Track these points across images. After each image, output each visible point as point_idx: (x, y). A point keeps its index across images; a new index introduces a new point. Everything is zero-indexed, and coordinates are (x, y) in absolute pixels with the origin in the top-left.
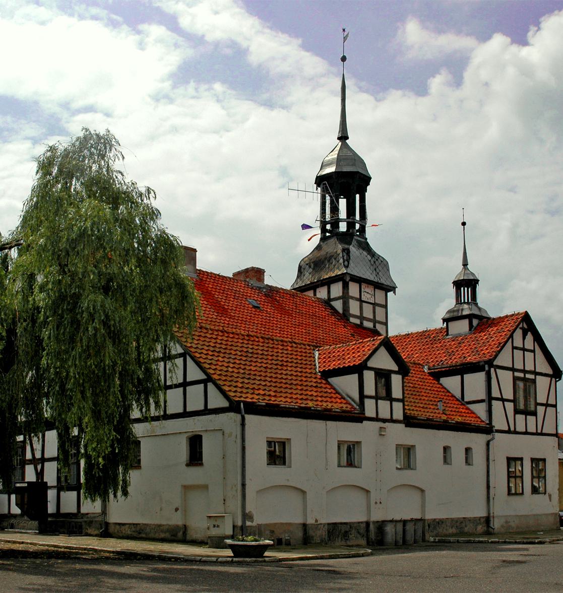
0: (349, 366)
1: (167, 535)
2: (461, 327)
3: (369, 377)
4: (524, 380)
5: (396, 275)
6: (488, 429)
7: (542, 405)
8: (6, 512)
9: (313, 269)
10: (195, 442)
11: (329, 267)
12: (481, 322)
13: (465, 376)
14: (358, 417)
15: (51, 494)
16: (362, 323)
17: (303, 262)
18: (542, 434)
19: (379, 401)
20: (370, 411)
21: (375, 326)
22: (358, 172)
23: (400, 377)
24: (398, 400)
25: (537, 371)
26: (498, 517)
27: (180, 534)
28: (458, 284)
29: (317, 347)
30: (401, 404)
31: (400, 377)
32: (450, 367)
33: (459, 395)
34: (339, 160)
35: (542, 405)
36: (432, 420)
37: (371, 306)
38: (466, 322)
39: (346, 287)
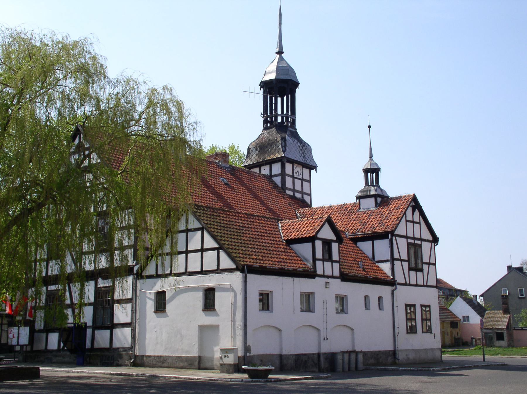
0: (306, 237)
1: (186, 364)
2: (369, 204)
3: (319, 244)
4: (414, 245)
5: (317, 157)
6: (392, 283)
7: (426, 263)
8: (43, 348)
9: (259, 151)
10: (209, 294)
11: (271, 151)
12: (383, 200)
13: (375, 242)
14: (311, 274)
15: (89, 332)
16: (294, 194)
17: (251, 146)
18: (427, 286)
19: (325, 263)
20: (319, 271)
21: (303, 197)
22: (291, 80)
23: (337, 244)
24: (336, 262)
25: (422, 238)
26: (401, 350)
27: (196, 363)
28: (366, 171)
29: (279, 220)
30: (338, 264)
31: (337, 244)
32: (364, 234)
33: (371, 256)
34: (279, 70)
35: (426, 263)
36: (357, 276)
37: (300, 181)
38: (373, 200)
39: (283, 167)
